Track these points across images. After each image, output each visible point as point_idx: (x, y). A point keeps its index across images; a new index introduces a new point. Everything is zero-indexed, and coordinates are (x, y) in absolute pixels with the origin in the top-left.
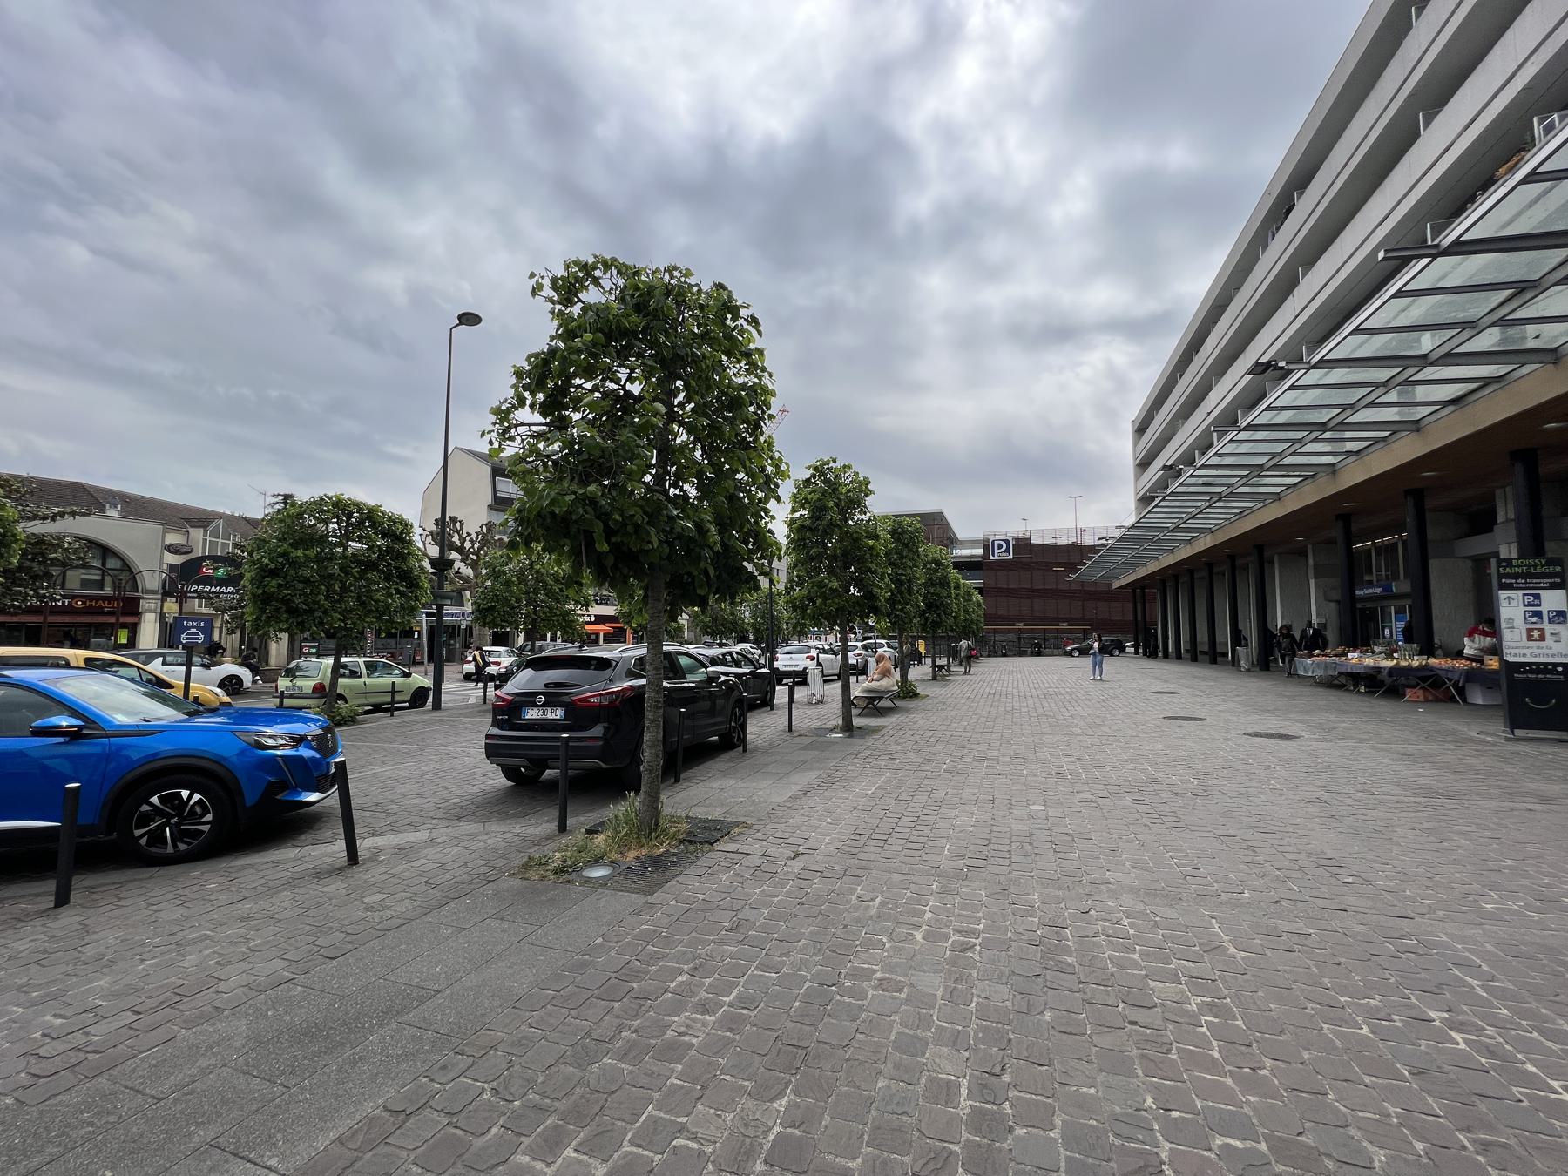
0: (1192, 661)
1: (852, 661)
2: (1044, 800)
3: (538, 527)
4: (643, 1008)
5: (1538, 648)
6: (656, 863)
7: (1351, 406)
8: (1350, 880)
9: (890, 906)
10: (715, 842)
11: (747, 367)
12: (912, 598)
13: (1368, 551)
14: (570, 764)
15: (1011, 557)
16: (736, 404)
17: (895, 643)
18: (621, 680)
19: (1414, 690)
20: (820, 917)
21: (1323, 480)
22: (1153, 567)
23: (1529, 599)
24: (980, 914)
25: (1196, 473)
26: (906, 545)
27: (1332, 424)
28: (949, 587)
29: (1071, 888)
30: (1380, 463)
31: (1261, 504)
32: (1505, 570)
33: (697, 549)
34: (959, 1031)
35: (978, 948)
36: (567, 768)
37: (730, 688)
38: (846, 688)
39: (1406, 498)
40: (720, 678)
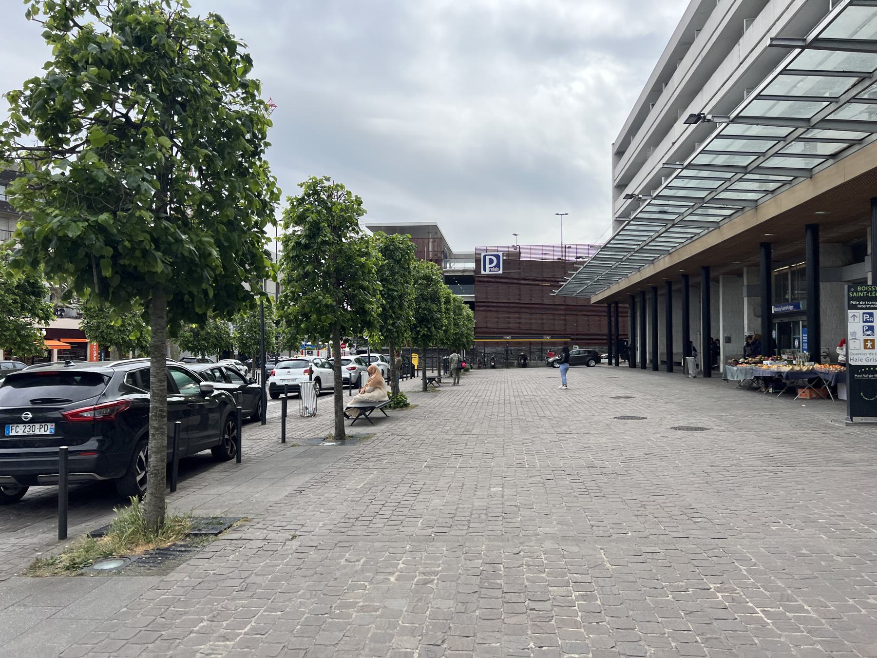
0: (654, 370)
1: (345, 374)
2: (503, 484)
3: (42, 250)
4: (173, 644)
5: (870, 354)
6: (165, 553)
7: (764, 154)
8: (699, 520)
9: (372, 563)
10: (220, 533)
11: (245, 95)
12: (403, 313)
13: (784, 275)
14: (70, 478)
15: (501, 272)
16: (234, 134)
17: (387, 357)
18: (114, 394)
19: (803, 390)
20: (315, 576)
21: (749, 213)
22: (623, 284)
23: (866, 316)
24: (441, 562)
25: (654, 202)
26: (398, 262)
27: (750, 168)
28: (439, 301)
29: (510, 540)
30: (789, 201)
31: (706, 231)
32: (853, 294)
33: (199, 270)
34: (416, 627)
35: (436, 581)
36: (67, 482)
37: (223, 402)
38: (339, 400)
39: (806, 232)
40: (213, 392)
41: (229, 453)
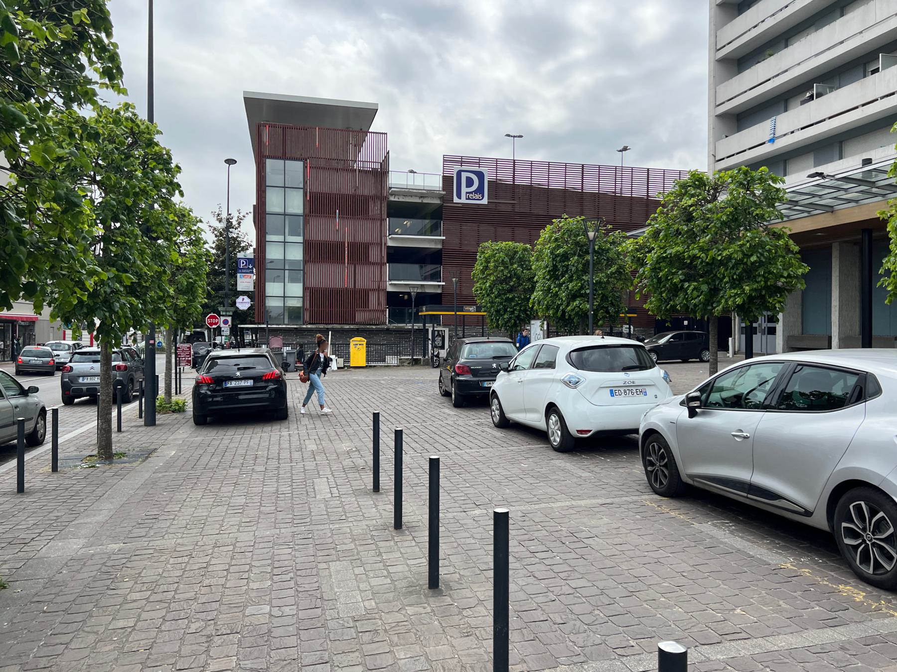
15: (485, 201)
41: (862, 503)
